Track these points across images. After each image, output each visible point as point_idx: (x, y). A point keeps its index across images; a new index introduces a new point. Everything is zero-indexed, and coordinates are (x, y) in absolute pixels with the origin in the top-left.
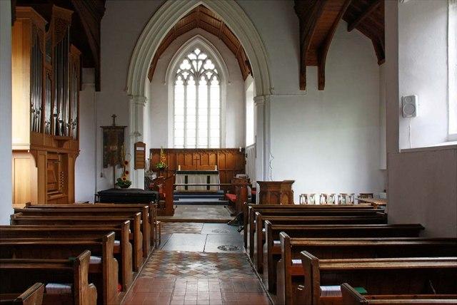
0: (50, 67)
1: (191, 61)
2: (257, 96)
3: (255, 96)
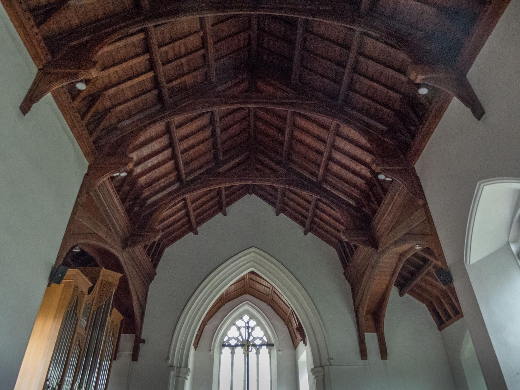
0: (83, 333)
1: (239, 328)
2: (315, 367)
3: (312, 367)
